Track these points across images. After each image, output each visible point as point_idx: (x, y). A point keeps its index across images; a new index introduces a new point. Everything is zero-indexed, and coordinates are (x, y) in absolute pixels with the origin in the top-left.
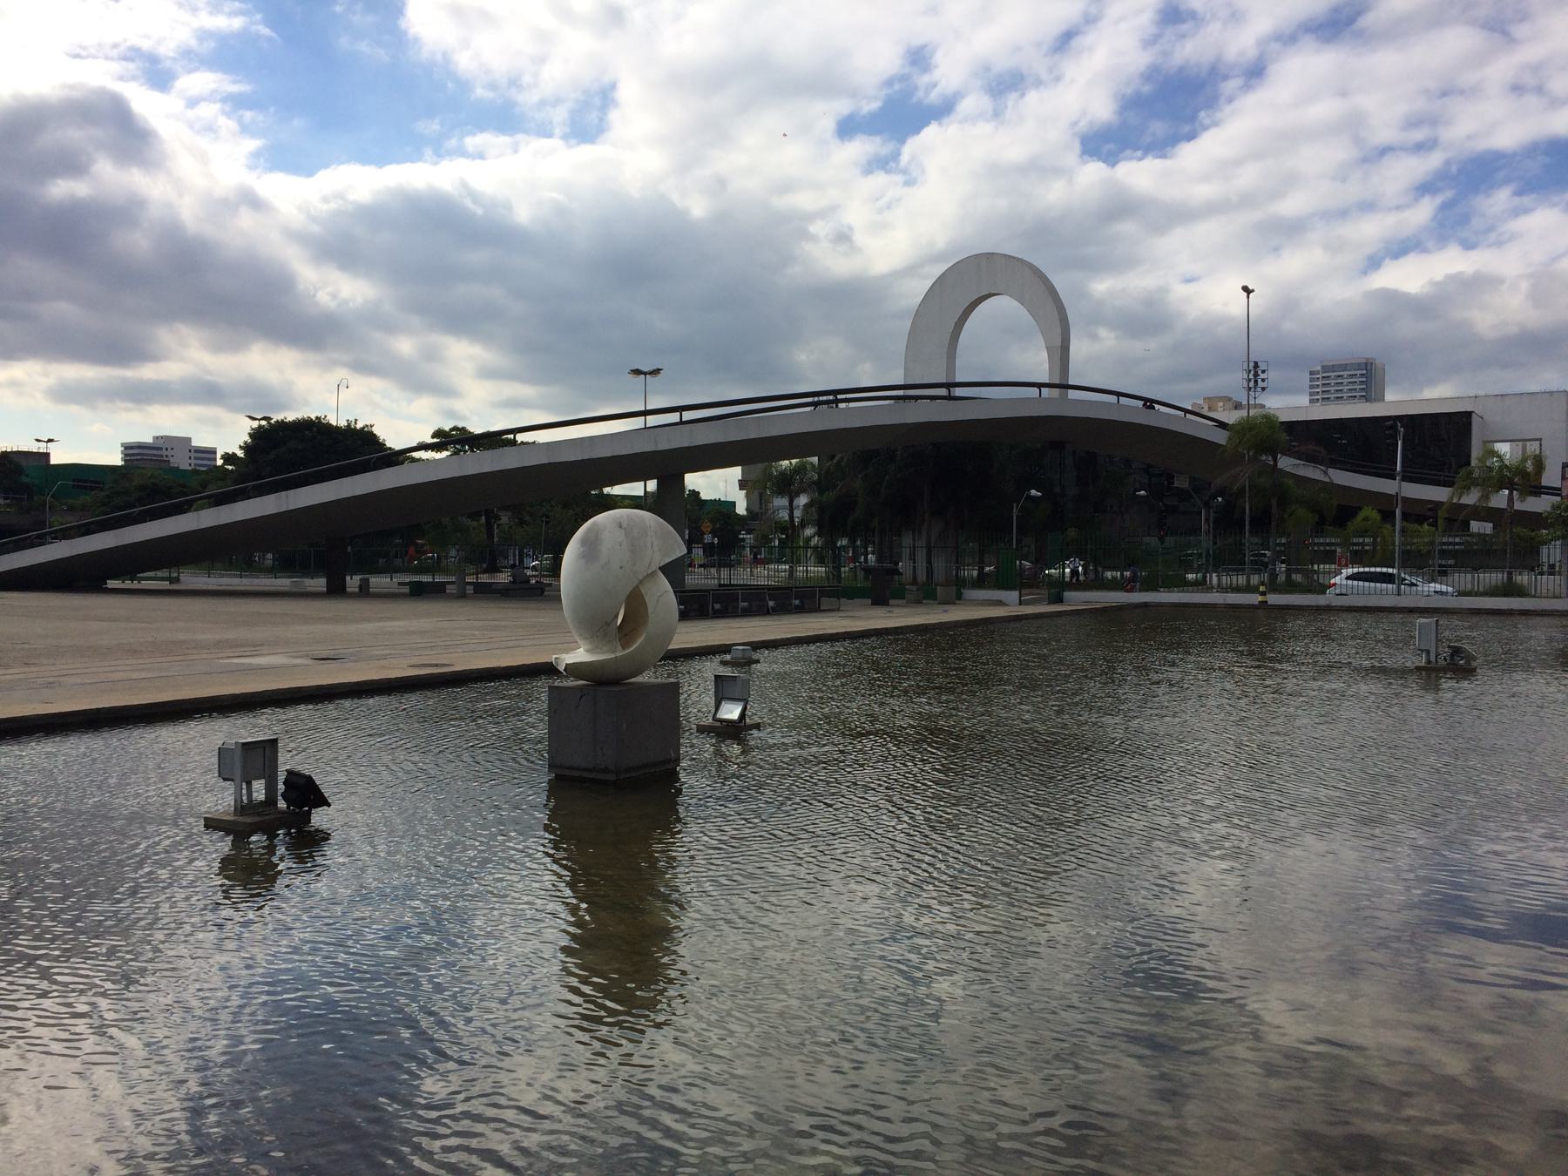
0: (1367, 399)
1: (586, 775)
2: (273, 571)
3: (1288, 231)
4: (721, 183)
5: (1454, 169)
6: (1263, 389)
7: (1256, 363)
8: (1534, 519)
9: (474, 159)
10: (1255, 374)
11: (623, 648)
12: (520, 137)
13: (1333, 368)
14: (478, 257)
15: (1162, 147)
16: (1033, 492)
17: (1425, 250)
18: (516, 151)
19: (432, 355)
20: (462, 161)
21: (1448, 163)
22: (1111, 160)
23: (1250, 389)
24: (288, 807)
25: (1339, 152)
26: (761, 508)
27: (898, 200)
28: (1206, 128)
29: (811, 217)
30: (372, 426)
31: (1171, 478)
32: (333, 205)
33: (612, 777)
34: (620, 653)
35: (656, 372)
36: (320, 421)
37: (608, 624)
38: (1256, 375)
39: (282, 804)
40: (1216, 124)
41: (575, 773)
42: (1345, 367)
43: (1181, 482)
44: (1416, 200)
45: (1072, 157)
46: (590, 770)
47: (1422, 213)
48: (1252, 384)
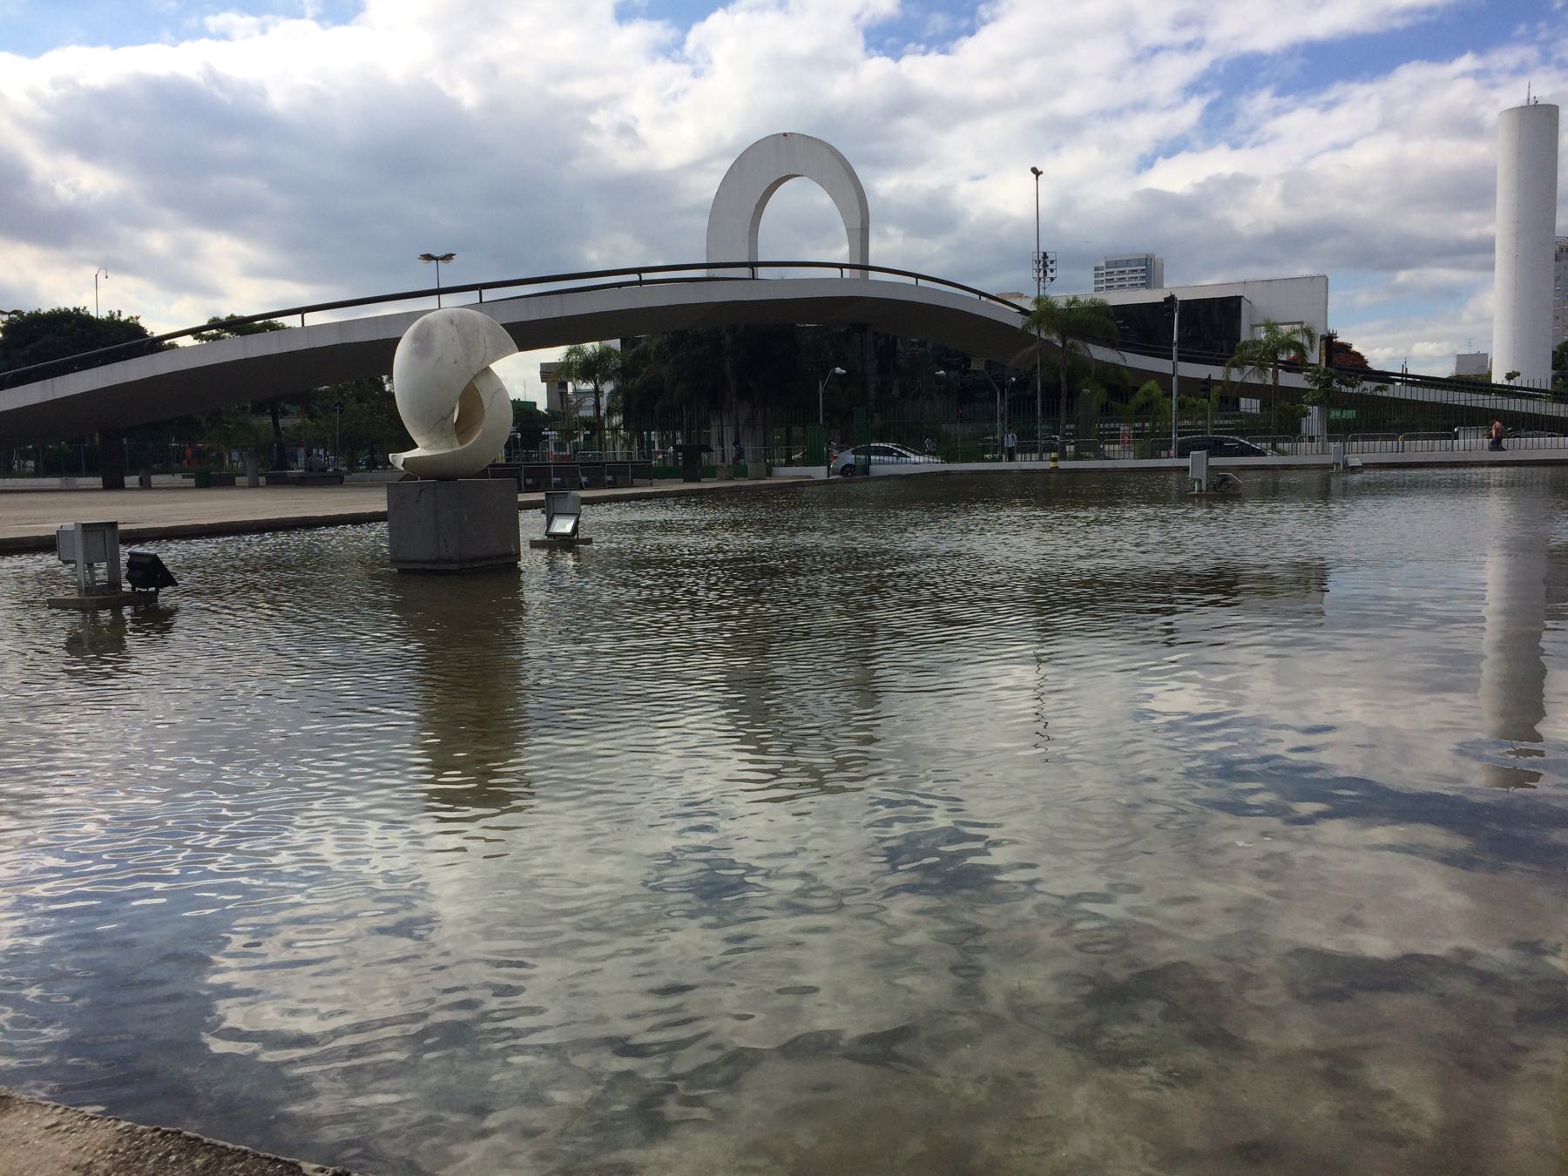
0: (1147, 286)
1: (429, 567)
2: (36, 474)
3: (1064, 130)
4: (491, 70)
5: (1221, 69)
6: (1052, 279)
7: (1045, 254)
8: (1295, 394)
9: (218, 40)
10: (1044, 263)
11: (461, 444)
12: (267, 18)
13: (1116, 264)
14: (237, 146)
15: (943, 42)
16: (838, 370)
17: (1193, 150)
18: (264, 31)
19: (188, 252)
20: (204, 43)
21: (1215, 63)
22: (896, 54)
23: (1040, 279)
24: (133, 589)
25: (1111, 51)
26: (562, 408)
27: (685, 91)
28: (984, 23)
29: (591, 107)
30: (137, 318)
31: (967, 361)
32: (63, 91)
33: (456, 567)
34: (458, 448)
35: (448, 257)
36: (78, 313)
37: (444, 419)
38: (1045, 265)
39: (127, 587)
40: (993, 19)
41: (419, 566)
42: (1128, 263)
43: (977, 365)
44: (1186, 100)
45: (856, 50)
46: (433, 562)
47: (1191, 113)
48: (1041, 274)
